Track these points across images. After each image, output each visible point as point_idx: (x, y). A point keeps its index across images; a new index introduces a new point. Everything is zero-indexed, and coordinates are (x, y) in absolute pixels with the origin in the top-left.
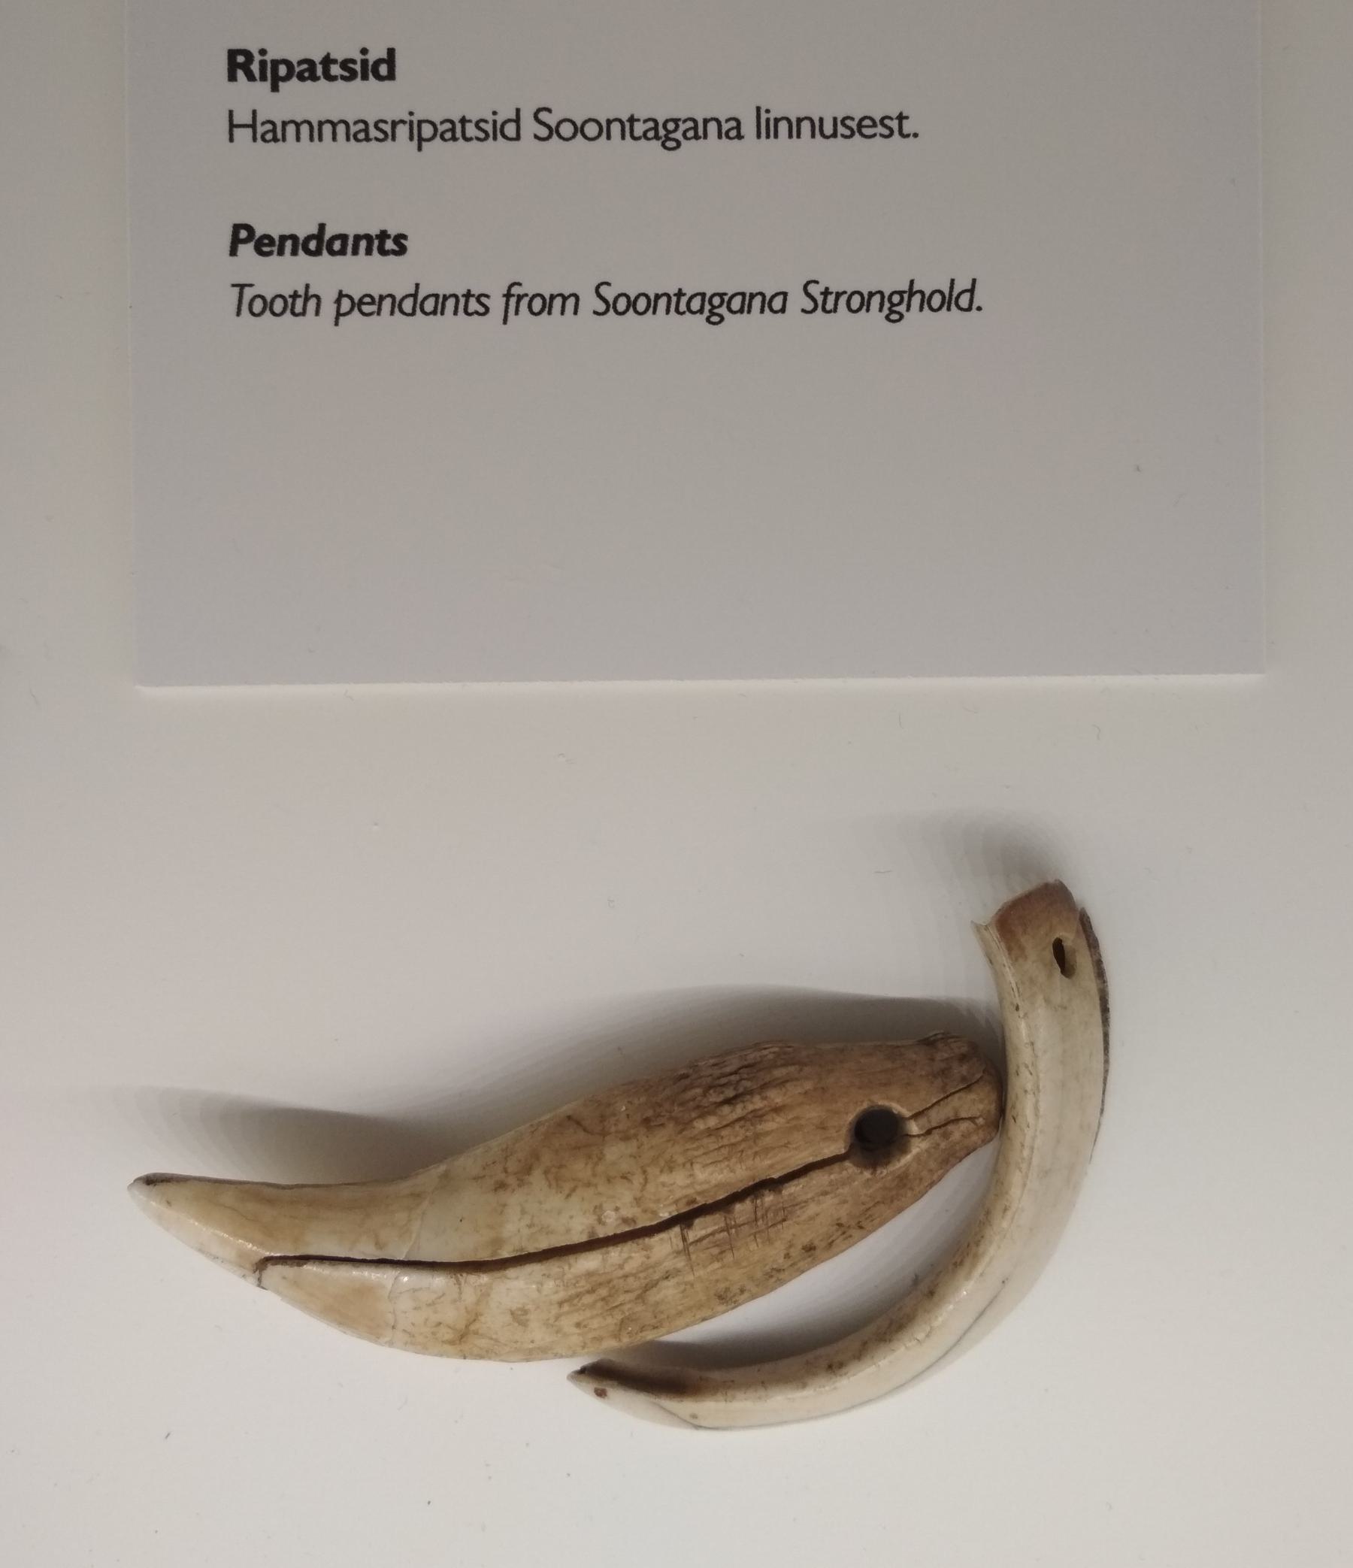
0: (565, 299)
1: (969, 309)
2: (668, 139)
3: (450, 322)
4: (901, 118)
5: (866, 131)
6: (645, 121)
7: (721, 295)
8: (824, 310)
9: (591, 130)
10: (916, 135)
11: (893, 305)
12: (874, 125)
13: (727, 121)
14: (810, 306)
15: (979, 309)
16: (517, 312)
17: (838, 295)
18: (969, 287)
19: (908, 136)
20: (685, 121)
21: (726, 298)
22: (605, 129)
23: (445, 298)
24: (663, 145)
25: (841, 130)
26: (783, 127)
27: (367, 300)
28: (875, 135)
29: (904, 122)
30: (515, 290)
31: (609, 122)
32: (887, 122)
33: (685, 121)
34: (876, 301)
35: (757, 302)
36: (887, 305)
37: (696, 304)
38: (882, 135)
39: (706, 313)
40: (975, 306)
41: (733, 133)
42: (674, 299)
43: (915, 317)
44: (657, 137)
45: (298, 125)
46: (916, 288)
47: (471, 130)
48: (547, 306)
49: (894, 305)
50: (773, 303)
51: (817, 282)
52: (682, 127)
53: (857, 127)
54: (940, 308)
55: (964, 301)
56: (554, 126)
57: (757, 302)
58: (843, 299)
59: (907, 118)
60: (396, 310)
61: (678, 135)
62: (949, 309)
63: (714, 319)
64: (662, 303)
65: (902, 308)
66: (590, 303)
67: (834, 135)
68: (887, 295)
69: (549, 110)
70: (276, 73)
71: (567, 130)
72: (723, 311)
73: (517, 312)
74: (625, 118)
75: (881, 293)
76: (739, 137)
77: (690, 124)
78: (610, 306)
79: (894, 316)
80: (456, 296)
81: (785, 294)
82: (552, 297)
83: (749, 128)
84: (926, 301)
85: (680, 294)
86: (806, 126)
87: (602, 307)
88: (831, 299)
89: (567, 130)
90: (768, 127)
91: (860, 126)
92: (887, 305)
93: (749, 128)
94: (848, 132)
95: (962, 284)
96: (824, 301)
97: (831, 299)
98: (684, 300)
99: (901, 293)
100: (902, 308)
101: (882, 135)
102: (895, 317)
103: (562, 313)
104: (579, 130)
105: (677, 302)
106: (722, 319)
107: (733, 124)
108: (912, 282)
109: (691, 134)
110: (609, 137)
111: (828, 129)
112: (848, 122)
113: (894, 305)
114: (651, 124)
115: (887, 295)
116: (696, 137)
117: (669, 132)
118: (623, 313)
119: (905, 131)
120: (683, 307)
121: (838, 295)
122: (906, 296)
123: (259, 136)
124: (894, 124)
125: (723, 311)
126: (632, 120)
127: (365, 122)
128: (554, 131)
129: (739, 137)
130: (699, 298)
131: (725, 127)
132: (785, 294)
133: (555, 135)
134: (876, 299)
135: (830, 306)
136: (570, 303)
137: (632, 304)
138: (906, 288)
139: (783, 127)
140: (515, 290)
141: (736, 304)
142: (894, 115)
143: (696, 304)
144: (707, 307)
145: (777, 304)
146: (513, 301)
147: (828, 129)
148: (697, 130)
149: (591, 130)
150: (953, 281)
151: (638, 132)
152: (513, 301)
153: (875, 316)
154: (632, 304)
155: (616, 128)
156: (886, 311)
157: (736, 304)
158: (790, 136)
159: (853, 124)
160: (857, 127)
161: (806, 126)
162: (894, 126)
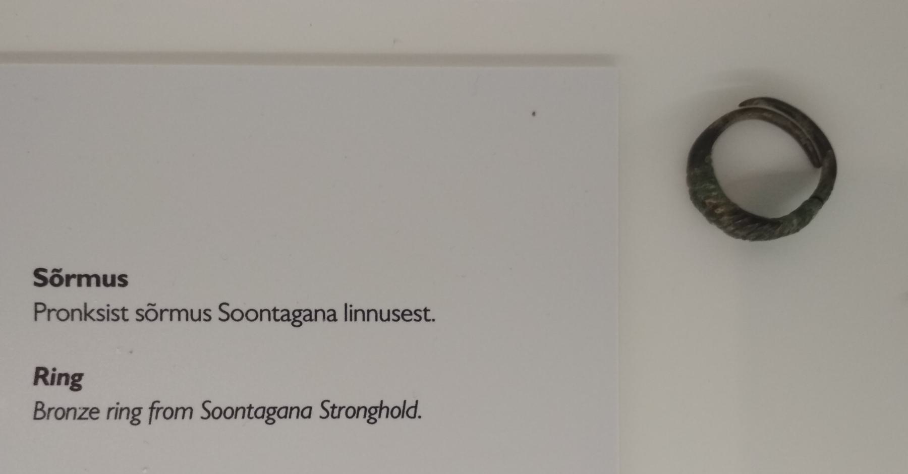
0: (185, 410)
1: (414, 417)
2: (295, 321)
4: (426, 310)
7: (274, 408)
9: (252, 315)
11: (269, 415)
12: (411, 314)
14: (325, 414)
15: (420, 417)
16: (156, 418)
17: (341, 409)
18: (414, 405)
22: (259, 315)
23: (292, 409)
24: (292, 324)
25: (392, 317)
26: (360, 314)
29: (126, 312)
30: (156, 405)
31: (262, 311)
32: (418, 313)
34: (362, 412)
35: (295, 412)
36: (368, 414)
37: (260, 413)
39: (265, 418)
40: (418, 415)
41: (331, 318)
42: (247, 410)
43: (384, 422)
44: (289, 320)
45: (179, 312)
47: (94, 315)
48: (174, 413)
49: (372, 414)
50: (304, 413)
52: (303, 314)
53: (402, 315)
55: (411, 413)
56: (245, 312)
57: (295, 412)
58: (343, 411)
61: (301, 319)
63: (270, 421)
64: (240, 412)
65: (376, 416)
66: (199, 412)
67: (388, 319)
68: (131, 410)
70: (59, 279)
71: (237, 315)
72: (275, 417)
73: (156, 418)
74: (271, 309)
75: (128, 408)
76: (335, 320)
77: (308, 313)
78: (211, 414)
79: (372, 420)
81: (311, 408)
82: (177, 409)
83: (340, 315)
84: (390, 412)
85: (250, 407)
86: (372, 314)
88: (336, 410)
89: (237, 315)
90: (351, 314)
91: (403, 314)
92: (368, 414)
93: (340, 315)
94: (396, 318)
96: (332, 412)
97: (336, 410)
98: (253, 411)
99: (376, 408)
100: (376, 416)
102: (372, 421)
103: (183, 417)
104: (245, 315)
105: (248, 412)
106: (274, 421)
107: (331, 313)
108: (382, 402)
109: (308, 318)
110: (261, 320)
111: (385, 317)
112: (396, 312)
113: (372, 414)
114: (285, 313)
115: (131, 410)
116: (311, 320)
118: (60, 419)
119: (428, 318)
120: (252, 415)
121: (341, 409)
124: (422, 314)
125: (275, 417)
126: (275, 310)
127: (288, 311)
128: (230, 316)
129: (335, 320)
131: (327, 315)
132: (311, 408)
134: (362, 411)
135: (336, 414)
136: (188, 412)
137: (223, 413)
139: (360, 314)
140: (156, 405)
141: (282, 413)
142: (422, 309)
143: (260, 413)
144: (266, 415)
145: (306, 413)
146: (155, 411)
148: (311, 316)
149: (252, 315)
150: (405, 402)
151: (278, 317)
152: (155, 411)
153: (361, 421)
154: (223, 413)
155: (265, 314)
156: (130, 419)
157: (282, 413)
158: (364, 320)
159: (399, 314)
160: (402, 315)
161: (372, 314)
162: (422, 315)
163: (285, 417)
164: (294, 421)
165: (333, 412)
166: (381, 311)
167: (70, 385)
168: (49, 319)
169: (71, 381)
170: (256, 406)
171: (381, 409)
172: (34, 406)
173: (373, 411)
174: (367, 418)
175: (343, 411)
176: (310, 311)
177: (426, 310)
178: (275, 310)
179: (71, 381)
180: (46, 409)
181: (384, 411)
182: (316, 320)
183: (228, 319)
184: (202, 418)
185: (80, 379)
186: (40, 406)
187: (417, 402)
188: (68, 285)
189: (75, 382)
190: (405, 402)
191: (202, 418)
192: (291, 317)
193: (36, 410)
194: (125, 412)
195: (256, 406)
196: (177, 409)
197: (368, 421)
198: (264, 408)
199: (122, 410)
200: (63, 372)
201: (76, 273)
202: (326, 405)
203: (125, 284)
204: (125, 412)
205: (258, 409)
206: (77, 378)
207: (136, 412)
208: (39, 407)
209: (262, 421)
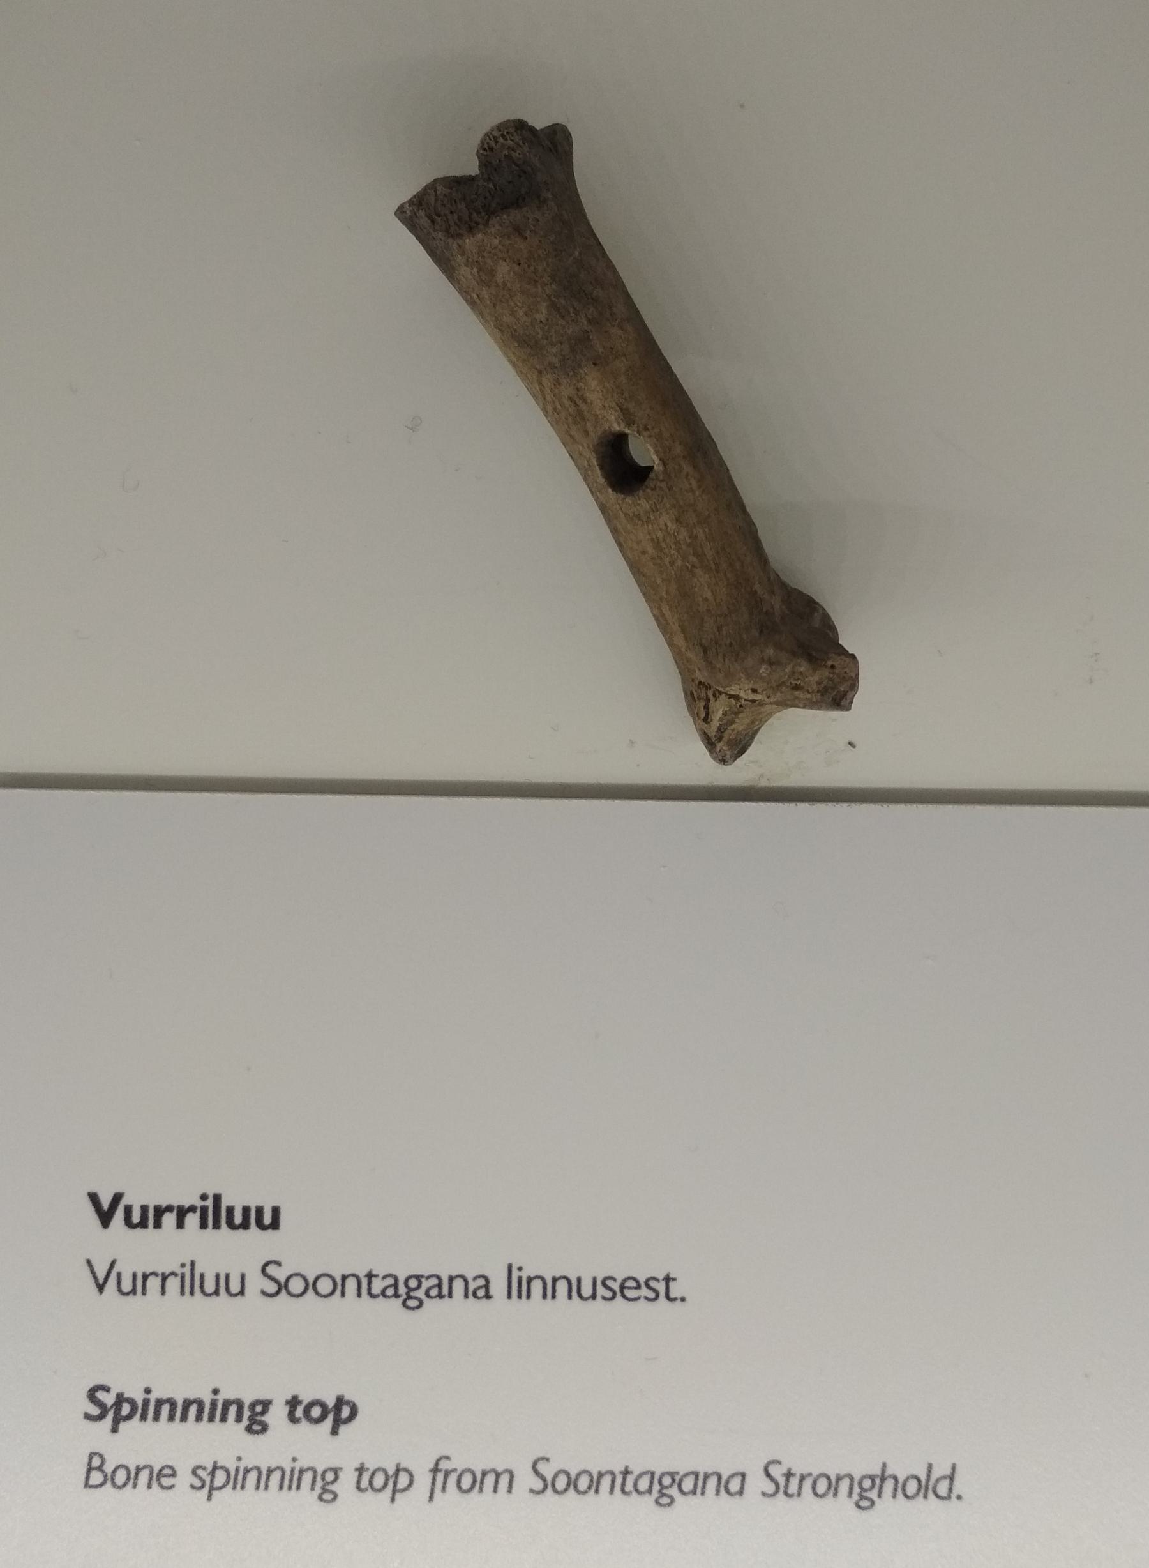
2: (409, 1297)
3: (141, 1496)
4: (668, 1279)
5: (629, 1293)
6: (384, 1277)
7: (672, 1475)
8: (786, 1494)
9: (325, 1286)
10: (683, 1299)
12: (639, 1287)
13: (475, 1278)
15: (959, 1497)
16: (444, 1489)
18: (948, 1472)
19: (675, 1299)
20: (428, 1278)
21: (677, 1478)
22: (339, 1286)
23: (706, 1476)
24: (404, 1304)
25: (601, 1291)
26: (537, 1286)
27: (167, 1471)
28: (639, 1298)
29: (671, 1284)
32: (652, 1283)
33: (428, 1278)
34: (844, 1486)
35: (712, 1483)
36: (857, 1490)
38: (646, 1298)
39: (655, 1494)
40: (954, 1496)
41: (481, 1293)
43: (888, 1505)
44: (396, 1295)
46: (889, 1472)
48: (478, 1482)
49: (868, 1489)
50: (729, 1485)
51: (779, 1463)
52: (426, 1284)
53: (619, 1289)
54: (125, 1485)
55: (943, 1489)
56: (283, 1281)
57: (712, 1483)
58: (808, 1484)
59: (674, 1279)
60: (722, 1489)
61: (420, 1294)
62: (925, 1497)
63: (664, 1500)
65: (873, 1495)
66: (526, 1480)
68: (320, 1472)
69: (278, 1264)
71: (296, 1286)
72: (674, 1492)
73: (444, 1489)
74: (362, 1274)
76: (488, 1296)
78: (548, 1485)
79: (864, 1503)
80: (612, 1473)
81: (743, 1476)
83: (498, 1287)
84: (900, 1488)
85: (626, 1472)
86: (562, 1287)
87: (539, 1485)
89: (296, 1286)
90: (520, 1286)
91: (622, 1287)
92: (857, 1490)
93: (498, 1287)
95: (939, 1471)
96: (784, 1484)
99: (872, 1478)
100: (873, 1495)
101: (646, 1298)
102: (665, 1500)
103: (495, 1491)
104: (311, 1286)
105: (623, 1481)
106: (672, 1500)
107: (482, 1282)
108: (884, 1465)
109: (434, 1292)
110: (343, 1294)
111: (587, 1291)
113: (868, 1489)
114: (391, 1281)
115: (320, 1472)
116: (440, 1296)
117: (410, 1290)
120: (629, 1487)
121: (802, 1479)
122: (878, 1481)
123: (470, 1293)
124: (661, 1287)
126: (370, 1276)
128: (283, 1286)
129: (488, 1296)
130: (692, 1477)
131: (472, 1286)
133: (284, 1291)
135: (793, 1487)
138: (878, 1472)
139: (537, 1286)
140: (444, 1465)
141: (688, 1485)
142: (661, 1277)
143: (644, 1484)
144: (656, 1487)
145: (735, 1486)
146: (440, 1477)
147: (587, 1291)
148: (442, 1289)
149: (325, 1286)
150: (930, 1466)
151: (376, 1290)
152: (440, 1477)
153: (843, 1504)
154: (572, 1483)
155: (351, 1284)
157: (688, 1485)
159: (615, 1286)
160: (619, 1289)
161: (562, 1287)
162: (661, 1289)
163: (694, 1492)
164: (711, 1503)
165: (786, 1486)
166: (579, 1280)
167: (245, 1422)
168: (163, 1293)
169: (247, 1413)
170: (636, 1470)
171: (883, 1480)
172: (86, 1460)
173: (867, 1484)
174: (855, 1497)
175: (808, 1484)
176: (439, 1278)
177: (668, 1279)
178: (370, 1276)
179: (247, 1413)
180: (108, 1468)
181: (889, 1485)
182: (450, 1295)
183: (278, 1293)
184: (532, 1491)
185: (263, 1412)
186: (96, 1462)
187: (954, 1468)
188: (158, 1225)
189: (339, 1413)
190: (930, 1466)
191: (532, 1491)
192: (402, 1290)
193: (90, 1469)
194: (308, 1477)
195: (636, 1470)
196: (138, 1470)
197: (320, 1498)
198: (653, 1474)
199: (247, 1471)
200: (232, 1397)
201: (175, 1204)
202: (775, 1471)
203: (275, 1225)
204: (308, 1477)
205: (641, 1475)
206: (259, 1409)
207: (330, 1477)
208: (95, 1464)
209: (649, 1500)
